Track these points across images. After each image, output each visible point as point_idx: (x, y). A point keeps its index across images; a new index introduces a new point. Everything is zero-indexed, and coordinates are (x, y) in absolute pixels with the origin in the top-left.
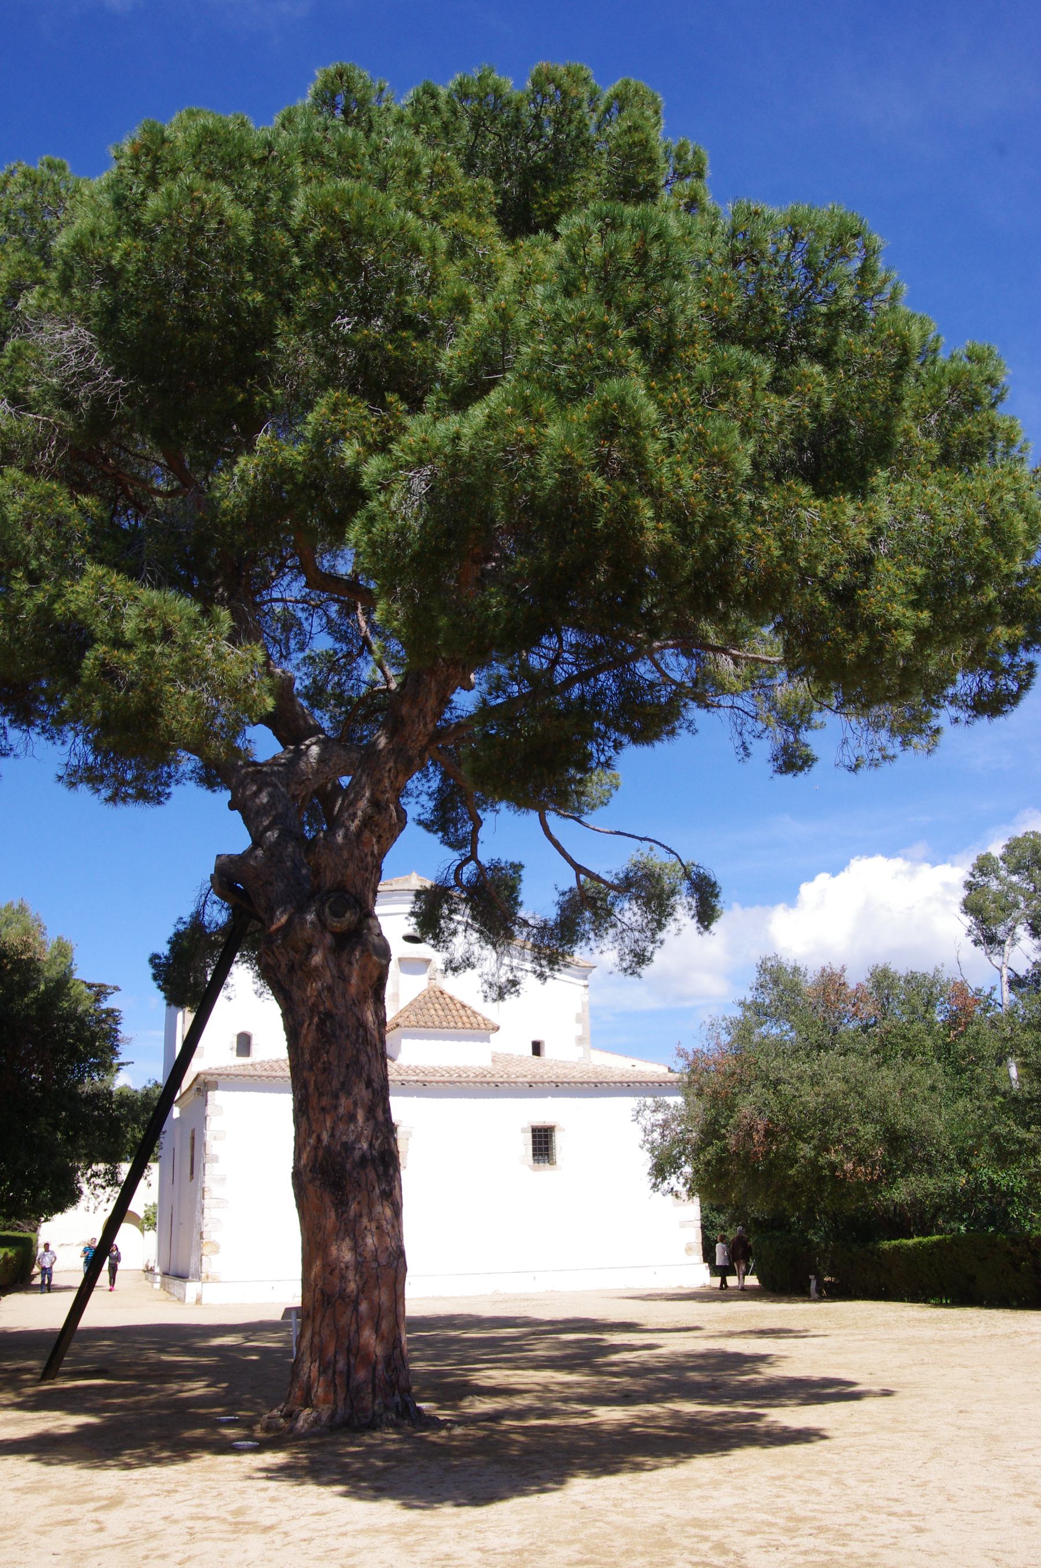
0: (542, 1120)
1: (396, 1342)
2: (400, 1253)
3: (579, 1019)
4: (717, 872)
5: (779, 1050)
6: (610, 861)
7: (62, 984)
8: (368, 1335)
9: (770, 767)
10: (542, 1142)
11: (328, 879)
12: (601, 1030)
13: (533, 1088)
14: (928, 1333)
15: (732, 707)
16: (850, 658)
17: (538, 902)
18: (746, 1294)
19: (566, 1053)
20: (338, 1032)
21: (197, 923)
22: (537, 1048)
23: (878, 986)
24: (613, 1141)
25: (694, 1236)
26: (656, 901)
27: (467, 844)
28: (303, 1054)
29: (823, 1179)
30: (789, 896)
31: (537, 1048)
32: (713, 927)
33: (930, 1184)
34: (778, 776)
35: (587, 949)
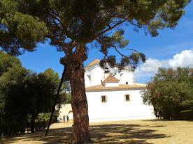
0: (103, 95)
1: (87, 130)
2: (88, 116)
5: (161, 81)
6: (128, 53)
7: (49, 80)
8: (82, 129)
10: (127, 97)
11: (74, 60)
12: (136, 80)
13: (125, 89)
14: (185, 126)
16: (136, 12)
17: (118, 61)
18: (162, 120)
19: (131, 83)
22: (127, 83)
24: (137, 96)
25: (153, 111)
26: (136, 60)
27: (106, 54)
29: (170, 102)
30: (172, 57)
31: (127, 83)
33: (188, 101)
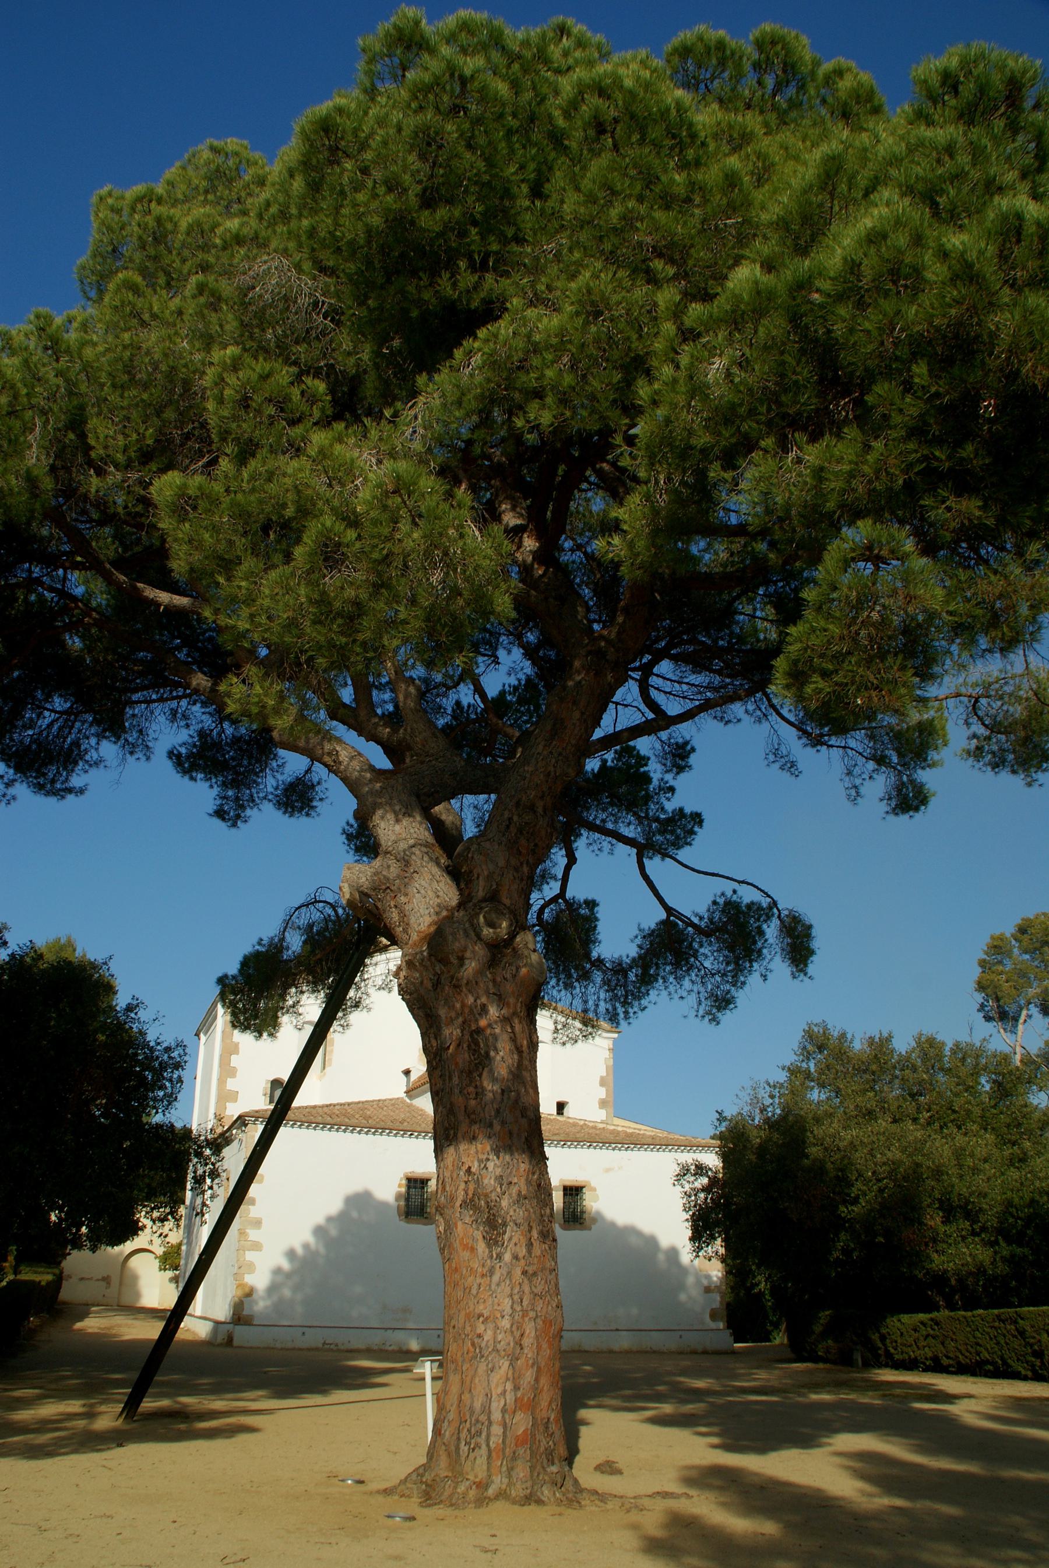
3: (603, 1082)
4: (811, 914)
6: (694, 899)
9: (884, 807)
15: (844, 747)
17: (617, 940)
20: (492, 1053)
21: (277, 947)
23: (925, 1056)
28: (450, 1078)
32: (811, 969)
34: (891, 818)
35: (664, 993)
